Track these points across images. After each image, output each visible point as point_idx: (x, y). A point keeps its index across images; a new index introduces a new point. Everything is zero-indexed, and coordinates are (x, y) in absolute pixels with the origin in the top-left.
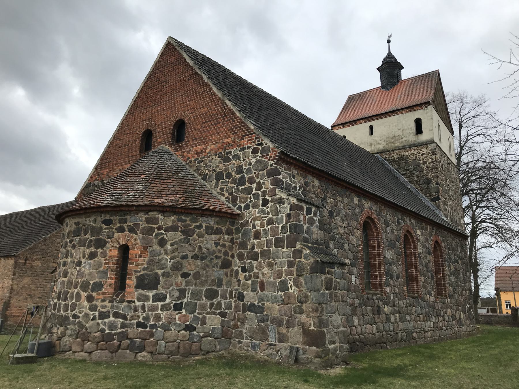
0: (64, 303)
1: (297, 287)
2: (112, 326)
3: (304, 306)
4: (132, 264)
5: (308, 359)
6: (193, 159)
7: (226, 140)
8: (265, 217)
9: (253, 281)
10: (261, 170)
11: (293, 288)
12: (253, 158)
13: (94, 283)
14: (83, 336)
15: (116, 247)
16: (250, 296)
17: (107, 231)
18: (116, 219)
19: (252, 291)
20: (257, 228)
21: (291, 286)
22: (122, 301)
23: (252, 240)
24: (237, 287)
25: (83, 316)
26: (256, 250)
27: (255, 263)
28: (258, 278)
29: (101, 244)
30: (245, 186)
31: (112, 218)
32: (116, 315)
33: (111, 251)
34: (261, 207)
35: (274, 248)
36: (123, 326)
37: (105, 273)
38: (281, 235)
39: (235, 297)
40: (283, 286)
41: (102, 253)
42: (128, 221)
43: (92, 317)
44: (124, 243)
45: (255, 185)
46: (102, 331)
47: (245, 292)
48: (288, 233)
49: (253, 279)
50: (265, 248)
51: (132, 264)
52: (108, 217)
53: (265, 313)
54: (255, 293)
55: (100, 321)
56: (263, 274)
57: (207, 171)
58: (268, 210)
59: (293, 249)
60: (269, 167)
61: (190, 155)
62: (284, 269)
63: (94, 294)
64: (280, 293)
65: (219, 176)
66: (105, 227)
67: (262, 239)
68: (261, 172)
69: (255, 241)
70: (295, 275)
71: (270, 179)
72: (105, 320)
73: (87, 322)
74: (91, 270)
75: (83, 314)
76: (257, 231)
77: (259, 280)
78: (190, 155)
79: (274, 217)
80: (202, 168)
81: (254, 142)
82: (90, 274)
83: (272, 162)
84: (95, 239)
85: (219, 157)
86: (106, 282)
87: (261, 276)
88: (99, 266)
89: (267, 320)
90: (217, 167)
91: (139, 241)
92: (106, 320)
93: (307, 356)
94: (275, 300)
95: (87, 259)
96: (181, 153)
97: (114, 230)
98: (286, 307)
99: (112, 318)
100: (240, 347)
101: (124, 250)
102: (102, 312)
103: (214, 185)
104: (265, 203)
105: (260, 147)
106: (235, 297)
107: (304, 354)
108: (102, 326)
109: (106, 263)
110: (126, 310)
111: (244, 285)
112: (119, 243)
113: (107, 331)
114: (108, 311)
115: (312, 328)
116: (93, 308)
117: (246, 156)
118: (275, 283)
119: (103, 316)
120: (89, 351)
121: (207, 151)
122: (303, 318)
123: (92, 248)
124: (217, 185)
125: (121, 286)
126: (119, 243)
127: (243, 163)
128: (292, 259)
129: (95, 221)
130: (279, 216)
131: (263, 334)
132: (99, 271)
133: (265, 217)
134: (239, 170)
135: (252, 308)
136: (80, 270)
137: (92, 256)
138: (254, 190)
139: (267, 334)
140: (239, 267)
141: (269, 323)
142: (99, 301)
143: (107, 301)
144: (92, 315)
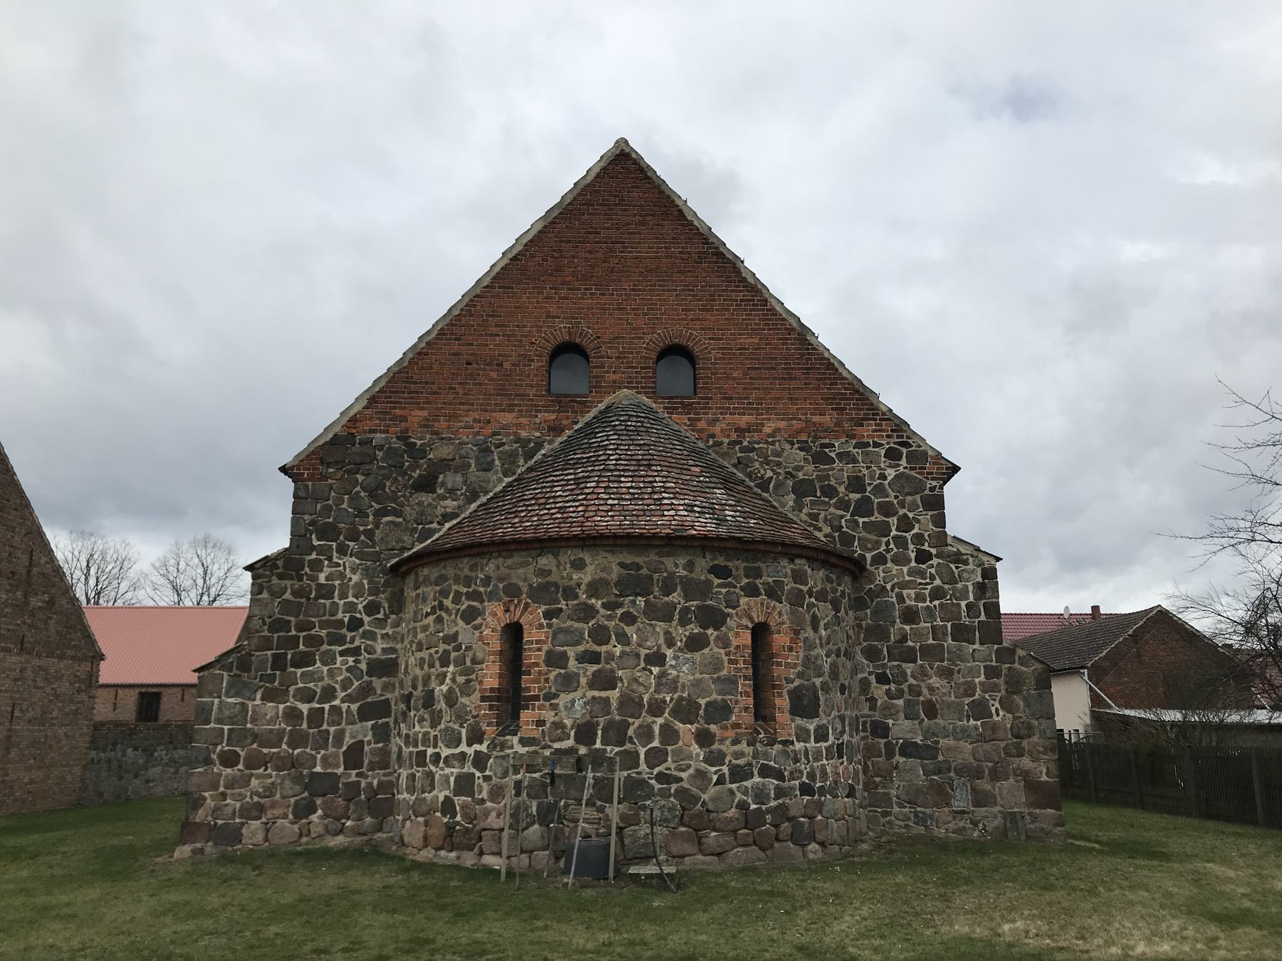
0: (713, 747)
1: (1009, 711)
2: (760, 796)
3: (1025, 743)
4: (779, 664)
5: (1042, 829)
6: (726, 441)
7: (816, 419)
8: (927, 584)
9: (908, 703)
10: (909, 494)
11: (1001, 713)
12: (890, 466)
13: (708, 704)
14: (694, 819)
15: (747, 627)
16: (902, 728)
17: (724, 590)
18: (737, 565)
19: (906, 718)
20: (908, 602)
21: (997, 710)
22: (771, 743)
23: (898, 624)
24: (866, 711)
25: (693, 776)
26: (910, 643)
27: (909, 668)
28: (919, 694)
29: (713, 618)
30: (873, 519)
31: (730, 564)
32: (765, 771)
33: (737, 634)
34: (913, 564)
35: (950, 641)
36: (780, 793)
37: (732, 681)
38: (965, 620)
39: (864, 730)
40: (980, 710)
41: (717, 637)
42: (765, 573)
43: (715, 778)
44: (762, 619)
45: (895, 519)
46: (743, 806)
47: (890, 722)
48: (983, 617)
49: (907, 696)
50: (931, 641)
51: (779, 664)
52: (721, 561)
53: (940, 758)
54: (916, 722)
55: (734, 786)
56: (931, 689)
57: (769, 474)
58: (933, 571)
59: (996, 647)
60: (927, 492)
61: (717, 429)
62: (977, 680)
63: (713, 728)
64: (972, 722)
65: (803, 489)
66: (717, 581)
67: (922, 624)
68: (909, 498)
69: (907, 628)
70: (1003, 692)
71: (930, 513)
72: (745, 783)
73: (704, 790)
74: (698, 676)
75: (691, 771)
76: (909, 608)
77: (921, 698)
78: (717, 429)
79: (946, 587)
80: (757, 465)
81: (888, 436)
82: (697, 683)
83: (934, 483)
84: (697, 607)
85: (801, 449)
86: (737, 702)
87: (925, 691)
88: (718, 666)
89: (949, 770)
90: (798, 468)
91: (785, 617)
92: (748, 784)
93: (1038, 825)
94: (964, 734)
95: (680, 650)
96: (689, 419)
97: (737, 590)
98: (987, 746)
99: (757, 779)
100: (890, 822)
101: (760, 632)
102: (739, 766)
103: (791, 503)
104: (923, 557)
105: (904, 450)
106: (864, 730)
107: (1033, 822)
108: (739, 796)
109: (731, 661)
110: (782, 760)
111: (886, 707)
112: (751, 619)
113: (753, 807)
114: (750, 765)
115: (1044, 778)
116: (715, 759)
117: (871, 460)
118: (961, 705)
119: (739, 774)
120: (719, 850)
121: (767, 430)
122: (1026, 762)
123: (692, 626)
124: (799, 507)
125: (763, 712)
126: (751, 619)
127: (865, 471)
128: (994, 664)
129: (690, 566)
130: (959, 585)
131: (941, 794)
132: (718, 678)
133: (927, 584)
134: (856, 484)
135: (909, 749)
136: (663, 674)
137: (695, 644)
138: (894, 528)
139: (947, 793)
140: (870, 673)
141: (952, 774)
142: (728, 742)
143: (744, 744)
144: (716, 773)
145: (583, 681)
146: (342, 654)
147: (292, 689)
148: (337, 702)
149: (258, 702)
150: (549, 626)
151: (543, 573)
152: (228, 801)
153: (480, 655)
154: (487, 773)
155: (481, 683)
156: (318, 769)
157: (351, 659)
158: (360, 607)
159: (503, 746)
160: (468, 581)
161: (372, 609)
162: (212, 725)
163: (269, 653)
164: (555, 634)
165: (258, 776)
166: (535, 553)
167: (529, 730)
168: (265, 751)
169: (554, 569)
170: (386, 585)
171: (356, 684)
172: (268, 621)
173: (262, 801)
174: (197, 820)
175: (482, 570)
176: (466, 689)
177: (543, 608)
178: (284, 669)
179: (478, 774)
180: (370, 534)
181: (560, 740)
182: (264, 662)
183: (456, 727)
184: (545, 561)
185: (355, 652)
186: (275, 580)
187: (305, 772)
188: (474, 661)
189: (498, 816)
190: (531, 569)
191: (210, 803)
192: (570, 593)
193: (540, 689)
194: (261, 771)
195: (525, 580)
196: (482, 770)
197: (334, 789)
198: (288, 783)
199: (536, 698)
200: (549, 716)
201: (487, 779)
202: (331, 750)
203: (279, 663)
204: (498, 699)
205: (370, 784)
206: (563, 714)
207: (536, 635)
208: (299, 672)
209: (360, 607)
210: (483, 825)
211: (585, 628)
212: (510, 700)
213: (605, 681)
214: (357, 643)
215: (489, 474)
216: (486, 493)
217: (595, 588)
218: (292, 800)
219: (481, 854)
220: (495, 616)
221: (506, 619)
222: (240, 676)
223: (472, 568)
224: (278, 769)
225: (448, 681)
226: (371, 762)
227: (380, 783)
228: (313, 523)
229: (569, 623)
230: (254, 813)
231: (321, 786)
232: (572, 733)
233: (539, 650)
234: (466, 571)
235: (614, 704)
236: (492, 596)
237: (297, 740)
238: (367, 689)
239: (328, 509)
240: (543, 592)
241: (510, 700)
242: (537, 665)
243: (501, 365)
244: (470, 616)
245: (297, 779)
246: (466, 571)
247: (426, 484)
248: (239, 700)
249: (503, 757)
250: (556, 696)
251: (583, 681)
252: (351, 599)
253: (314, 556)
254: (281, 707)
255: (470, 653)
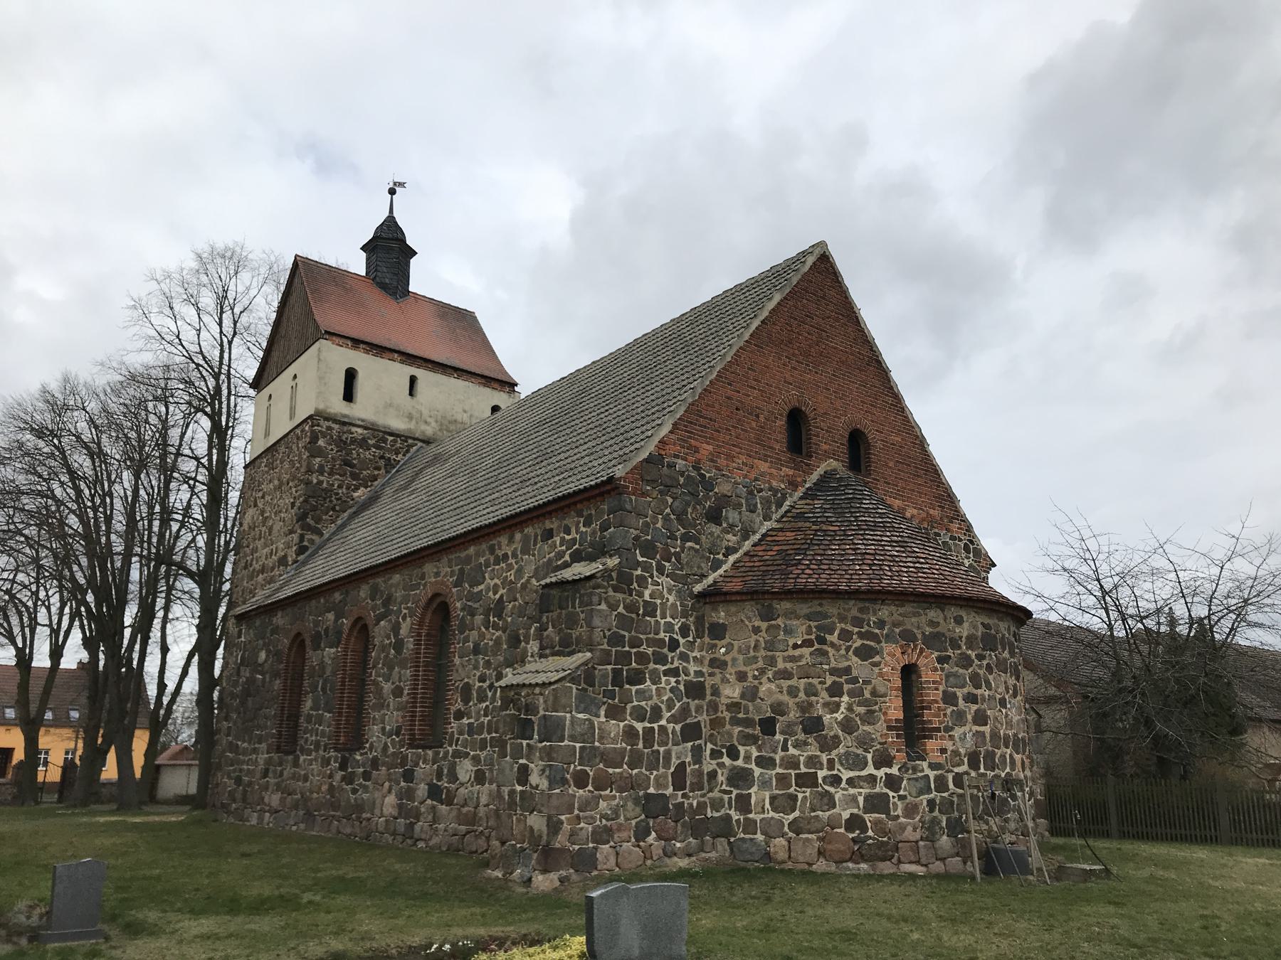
145: (969, 717)
146: (666, 673)
147: (629, 706)
148: (663, 722)
149: (603, 719)
150: (942, 669)
151: (932, 623)
152: (582, 825)
153: (881, 690)
154: (902, 793)
155: (885, 714)
156: (651, 790)
157: (673, 680)
158: (676, 628)
159: (915, 769)
160: (858, 622)
161: (684, 631)
162: (566, 743)
163: (609, 667)
164: (947, 676)
165: (605, 798)
166: (926, 605)
167: (935, 757)
168: (611, 771)
169: (942, 621)
170: (693, 609)
171: (678, 705)
172: (608, 634)
173: (609, 824)
174: (558, 845)
175: (875, 614)
176: (869, 718)
177: (936, 654)
178: (621, 687)
179: (891, 794)
180: (677, 555)
181: (959, 765)
182: (605, 676)
183: (860, 751)
184: (933, 614)
185: (674, 672)
186: (611, 593)
187: (641, 793)
188: (874, 693)
189: (915, 830)
190: (923, 619)
191: (567, 827)
192: (955, 644)
193: (940, 723)
194: (608, 792)
195: (918, 628)
196: (896, 790)
197: (665, 811)
198: (630, 805)
199: (938, 730)
200: (949, 746)
201: (901, 798)
202: (662, 770)
203: (617, 680)
204: (924, 729)
205: (691, 805)
206: (959, 744)
207: (931, 674)
208: (634, 688)
209: (676, 628)
210: (899, 838)
211: (967, 673)
212: (913, 730)
213: (981, 719)
214: (676, 664)
215: (754, 515)
216: (754, 533)
217: (971, 641)
218: (634, 822)
219: (900, 862)
220: (891, 658)
221: (906, 660)
222: (586, 690)
223: (861, 610)
224: (621, 790)
225: (842, 709)
226: (692, 783)
227: (698, 803)
228: (637, 538)
229: (956, 669)
230: (605, 837)
231: (654, 807)
232: (966, 760)
233: (937, 689)
234: (854, 612)
235: (988, 735)
236: (889, 638)
237: (635, 761)
238: (685, 711)
239: (647, 525)
240: (934, 641)
241: (913, 730)
242: (937, 702)
243: (757, 416)
244: (865, 653)
245: (637, 801)
246: (854, 612)
247: (714, 516)
248: (587, 716)
249: (916, 779)
250: (952, 729)
251: (969, 717)
252: (669, 619)
253: (639, 572)
254: (622, 724)
255: (869, 687)
